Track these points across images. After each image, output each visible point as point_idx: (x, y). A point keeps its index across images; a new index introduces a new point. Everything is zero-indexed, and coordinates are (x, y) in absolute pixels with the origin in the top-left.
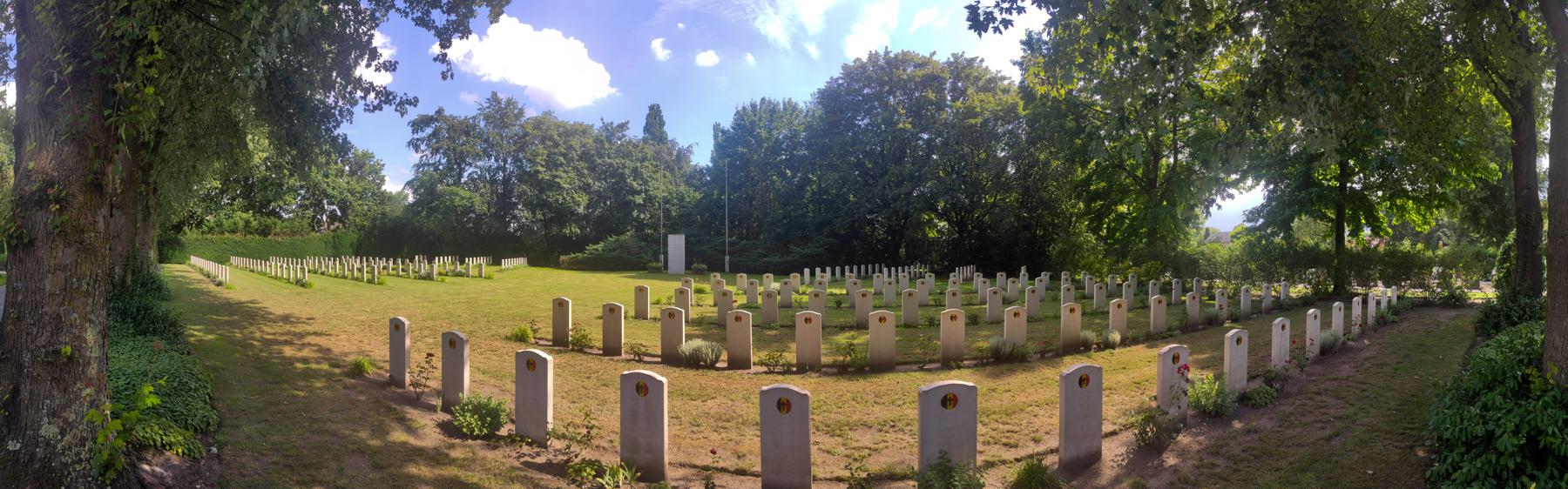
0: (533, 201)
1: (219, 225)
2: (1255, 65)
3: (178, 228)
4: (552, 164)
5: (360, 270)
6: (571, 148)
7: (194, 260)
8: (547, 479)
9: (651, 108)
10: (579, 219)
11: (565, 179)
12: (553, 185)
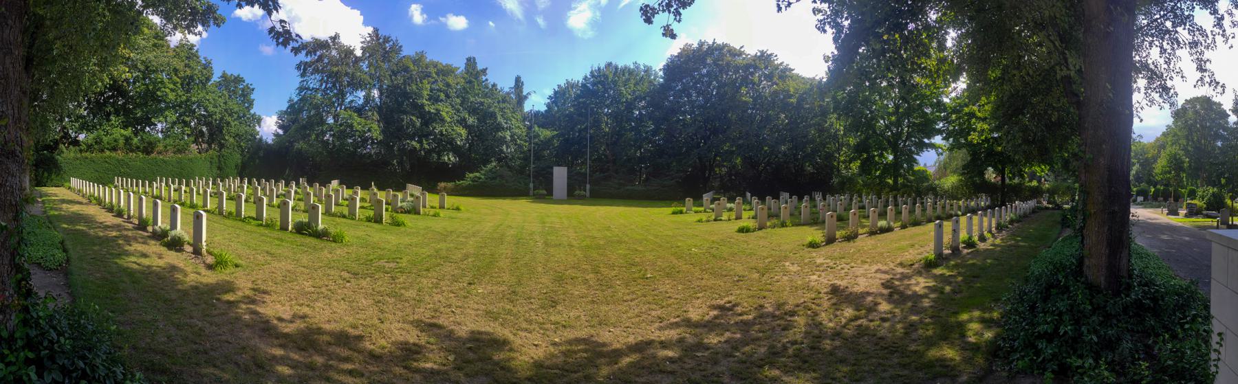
0: (398, 134)
1: (98, 141)
2: (406, 119)
3: (53, 147)
4: (434, 99)
5: (236, 199)
6: (448, 85)
7: (75, 182)
8: (349, 380)
9: (469, 60)
10: (456, 150)
11: (446, 111)
12: (437, 117)
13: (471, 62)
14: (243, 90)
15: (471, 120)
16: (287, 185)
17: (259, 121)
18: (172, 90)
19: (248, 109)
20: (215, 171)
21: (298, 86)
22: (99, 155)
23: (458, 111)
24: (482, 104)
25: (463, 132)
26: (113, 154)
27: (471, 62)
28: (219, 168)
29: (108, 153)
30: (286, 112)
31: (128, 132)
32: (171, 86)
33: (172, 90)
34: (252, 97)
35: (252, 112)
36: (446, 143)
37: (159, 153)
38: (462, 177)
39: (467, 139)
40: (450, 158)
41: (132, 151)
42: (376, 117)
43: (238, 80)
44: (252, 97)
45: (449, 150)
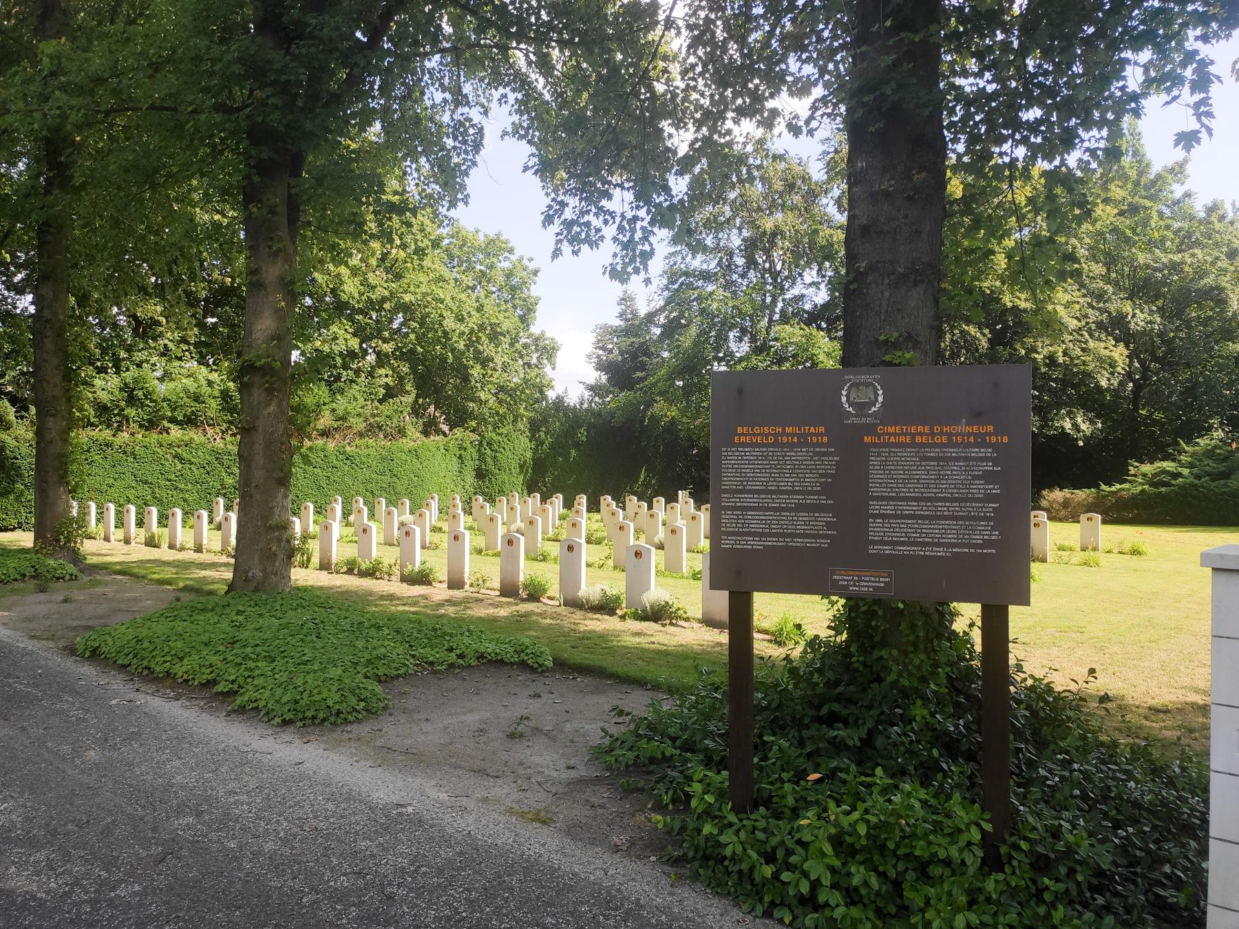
10: (1092, 400)
13: (1176, 145)
14: (509, 275)
15: (1141, 318)
17: (548, 351)
20: (470, 477)
23: (1100, 296)
24: (1175, 267)
25: (1119, 354)
26: (195, 435)
27: (1176, 145)
28: (481, 474)
29: (176, 433)
30: (615, 331)
34: (535, 291)
35: (535, 329)
36: (1073, 387)
37: (325, 433)
38: (1120, 474)
39: (1129, 375)
40: (1079, 425)
44: (535, 291)
45: (1070, 403)
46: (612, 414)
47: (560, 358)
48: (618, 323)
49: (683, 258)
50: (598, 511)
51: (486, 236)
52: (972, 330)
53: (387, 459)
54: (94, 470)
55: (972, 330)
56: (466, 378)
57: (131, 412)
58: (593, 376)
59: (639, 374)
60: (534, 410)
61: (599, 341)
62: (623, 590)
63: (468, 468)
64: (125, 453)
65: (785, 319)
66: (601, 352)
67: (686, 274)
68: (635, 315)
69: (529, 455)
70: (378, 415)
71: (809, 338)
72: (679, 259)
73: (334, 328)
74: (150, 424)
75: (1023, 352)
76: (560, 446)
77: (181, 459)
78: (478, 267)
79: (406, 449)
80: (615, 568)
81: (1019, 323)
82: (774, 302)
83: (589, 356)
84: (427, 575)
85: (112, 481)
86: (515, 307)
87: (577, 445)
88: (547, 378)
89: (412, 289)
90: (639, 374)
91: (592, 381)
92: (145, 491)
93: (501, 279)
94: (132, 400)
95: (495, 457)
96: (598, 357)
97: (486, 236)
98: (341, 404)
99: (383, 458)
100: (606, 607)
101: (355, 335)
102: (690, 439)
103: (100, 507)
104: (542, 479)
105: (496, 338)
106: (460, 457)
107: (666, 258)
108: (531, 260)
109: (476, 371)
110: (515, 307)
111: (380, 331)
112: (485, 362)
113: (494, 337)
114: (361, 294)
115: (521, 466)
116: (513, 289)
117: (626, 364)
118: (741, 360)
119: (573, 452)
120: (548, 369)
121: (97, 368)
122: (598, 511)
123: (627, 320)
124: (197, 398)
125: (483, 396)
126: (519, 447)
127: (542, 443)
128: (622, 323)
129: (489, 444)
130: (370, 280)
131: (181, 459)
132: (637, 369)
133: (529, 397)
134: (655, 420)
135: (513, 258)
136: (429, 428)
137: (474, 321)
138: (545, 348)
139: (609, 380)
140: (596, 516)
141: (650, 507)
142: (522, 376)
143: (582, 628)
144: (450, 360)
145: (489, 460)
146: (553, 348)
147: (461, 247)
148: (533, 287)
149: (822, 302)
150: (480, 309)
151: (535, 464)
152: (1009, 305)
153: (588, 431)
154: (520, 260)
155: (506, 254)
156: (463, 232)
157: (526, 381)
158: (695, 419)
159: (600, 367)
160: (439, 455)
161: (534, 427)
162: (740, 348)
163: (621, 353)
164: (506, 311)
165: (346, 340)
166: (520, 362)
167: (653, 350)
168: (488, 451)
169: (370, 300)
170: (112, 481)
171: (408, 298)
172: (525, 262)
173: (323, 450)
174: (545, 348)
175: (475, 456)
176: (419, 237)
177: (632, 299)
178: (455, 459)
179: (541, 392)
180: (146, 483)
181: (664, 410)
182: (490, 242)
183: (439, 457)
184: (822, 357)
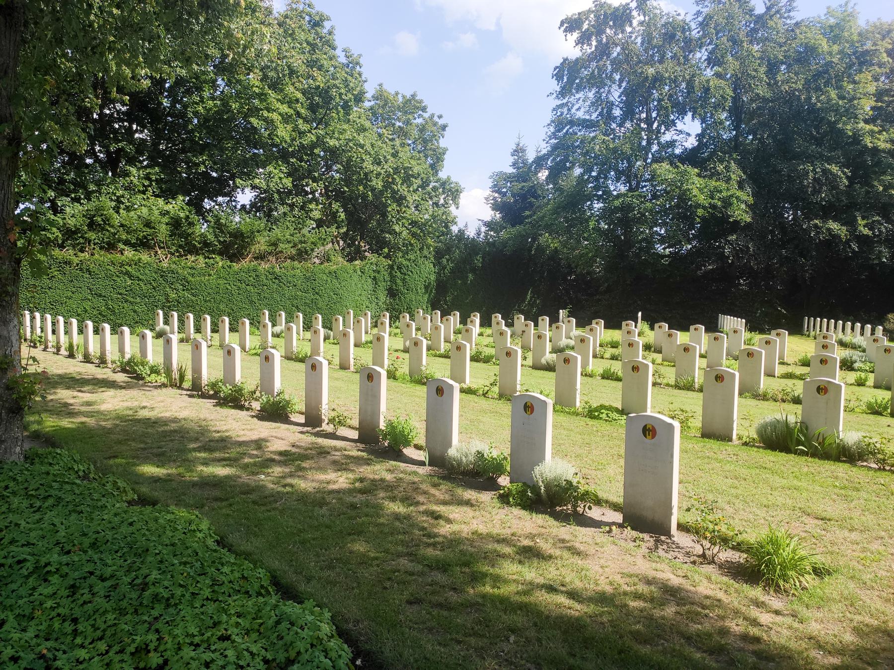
2: (811, 171)
14: (422, 129)
16: (464, 321)
17: (454, 193)
18: (286, 119)
19: (434, 168)
20: (383, 296)
21: (549, 116)
22: (101, 256)
26: (145, 257)
28: (392, 293)
29: (129, 253)
30: (509, 178)
31: (177, 206)
32: (284, 108)
33: (286, 119)
34: (443, 143)
35: (442, 175)
37: (261, 257)
41: (192, 250)
42: (736, 173)
43: (412, 105)
44: (443, 143)
46: (504, 243)
47: (463, 199)
48: (511, 170)
49: (569, 110)
50: (490, 325)
51: (404, 97)
52: (834, 169)
53: (310, 278)
54: (54, 284)
55: (834, 169)
56: (384, 215)
57: (92, 235)
58: (489, 214)
59: (527, 213)
60: (440, 241)
61: (495, 186)
62: (507, 452)
63: (381, 288)
64: (81, 270)
65: (656, 160)
66: (496, 195)
67: (572, 123)
68: (524, 162)
69: (433, 277)
70: (305, 242)
71: (683, 174)
72: (565, 110)
73: (270, 168)
74: (110, 247)
75: (881, 189)
76: (459, 270)
77: (130, 276)
78: (398, 124)
79: (327, 271)
80: (501, 396)
81: (878, 163)
82: (649, 143)
83: (486, 199)
84: (284, 408)
85: (70, 294)
86: (426, 156)
87: (474, 270)
88: (452, 216)
89: (336, 135)
90: (527, 213)
91: (488, 218)
92: (100, 303)
93: (415, 133)
94: (92, 225)
95: (404, 279)
96: (494, 199)
97: (404, 97)
98: (277, 232)
99: (307, 279)
100: (480, 475)
101: (289, 175)
102: (569, 266)
103: (42, 317)
104: (446, 297)
105: (409, 179)
106: (375, 278)
107: (554, 110)
108: (440, 117)
109: (393, 207)
110: (426, 156)
111: (310, 172)
112: (400, 200)
113: (407, 179)
114: (293, 140)
115: (426, 287)
116: (425, 141)
117: (517, 201)
118: (618, 197)
119: (471, 276)
120: (453, 208)
121: (72, 198)
122: (490, 325)
123: (518, 168)
124: (148, 224)
125: (397, 228)
126: (426, 271)
127: (444, 268)
128: (514, 171)
129: (399, 268)
130: (300, 126)
131: (130, 276)
132: (526, 209)
133: (436, 230)
134: (541, 249)
135: (426, 115)
136: (353, 255)
137: (388, 167)
138: (450, 190)
139: (502, 218)
140: (488, 331)
141: (536, 325)
142: (431, 213)
143: (445, 529)
144: (370, 198)
145: (398, 281)
146: (457, 191)
147: (383, 107)
148: (441, 141)
149: (690, 147)
150: (395, 155)
151: (438, 285)
152: (870, 145)
153: (483, 258)
154: (433, 116)
155: (420, 112)
156: (385, 94)
157: (433, 217)
158: (574, 250)
159: (496, 207)
160: (358, 277)
161: (439, 255)
162: (619, 188)
163: (513, 195)
164: (419, 159)
165: (280, 178)
166: (431, 203)
167: (540, 192)
168: (398, 274)
169: (302, 146)
170: (70, 294)
171: (332, 143)
172: (436, 119)
173: (255, 270)
174: (450, 190)
175: (387, 278)
176: (343, 91)
177: (523, 150)
178: (369, 280)
179: (447, 227)
180: (100, 296)
181: (548, 241)
182: (407, 102)
183: (355, 278)
184: (695, 192)
